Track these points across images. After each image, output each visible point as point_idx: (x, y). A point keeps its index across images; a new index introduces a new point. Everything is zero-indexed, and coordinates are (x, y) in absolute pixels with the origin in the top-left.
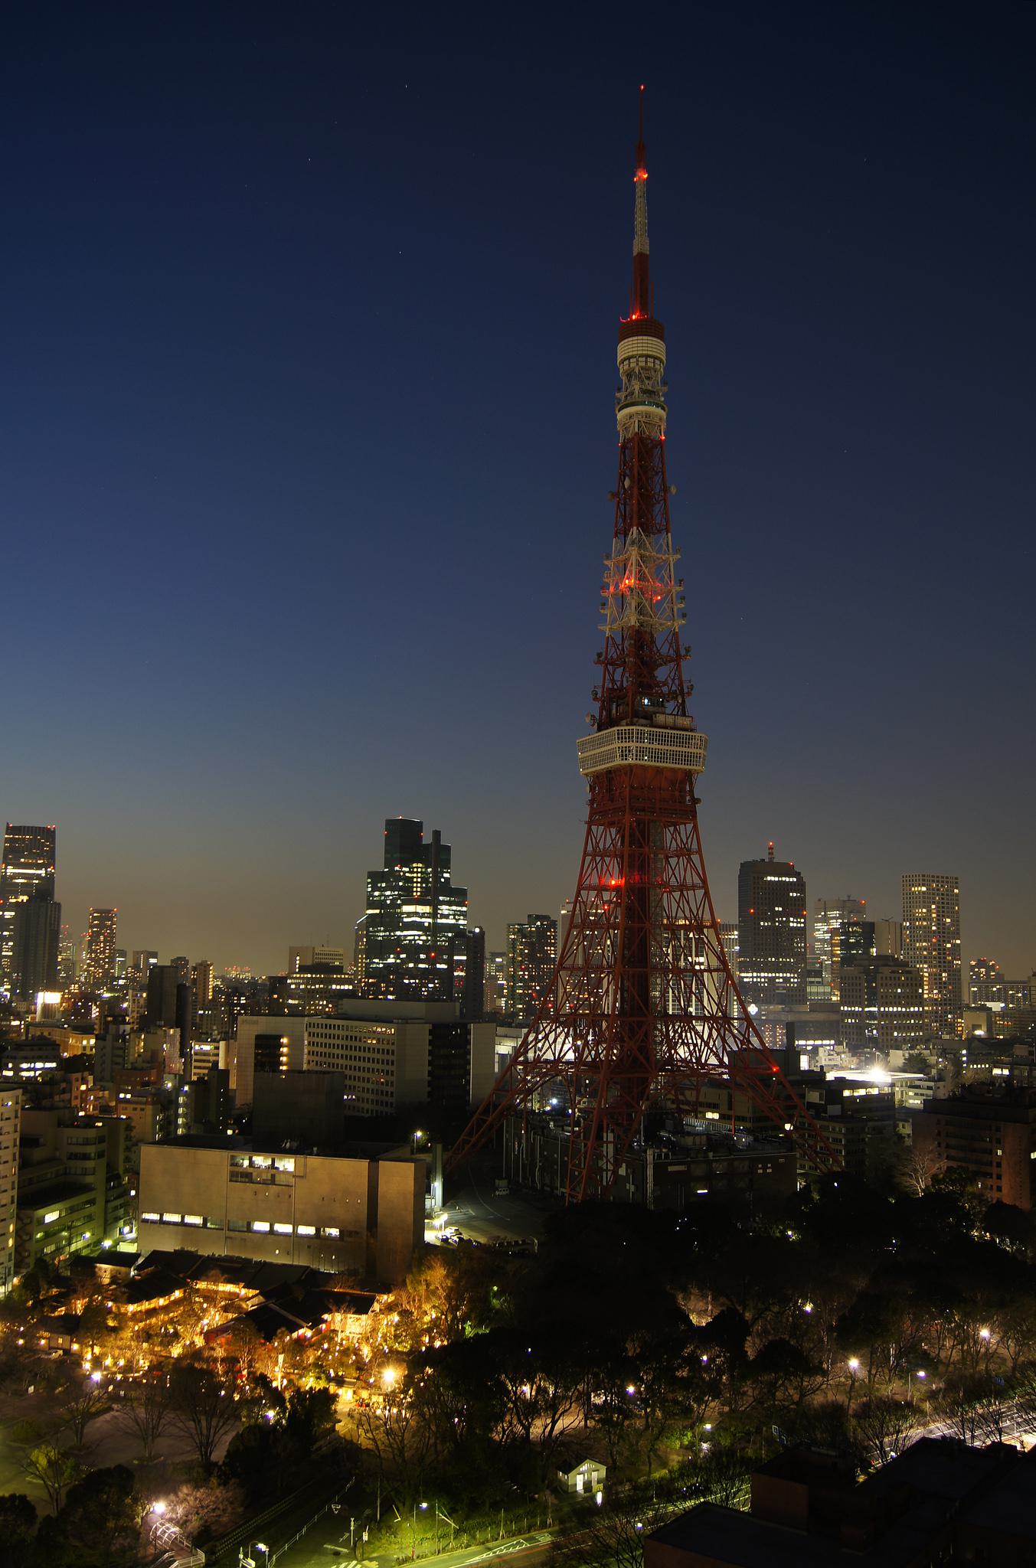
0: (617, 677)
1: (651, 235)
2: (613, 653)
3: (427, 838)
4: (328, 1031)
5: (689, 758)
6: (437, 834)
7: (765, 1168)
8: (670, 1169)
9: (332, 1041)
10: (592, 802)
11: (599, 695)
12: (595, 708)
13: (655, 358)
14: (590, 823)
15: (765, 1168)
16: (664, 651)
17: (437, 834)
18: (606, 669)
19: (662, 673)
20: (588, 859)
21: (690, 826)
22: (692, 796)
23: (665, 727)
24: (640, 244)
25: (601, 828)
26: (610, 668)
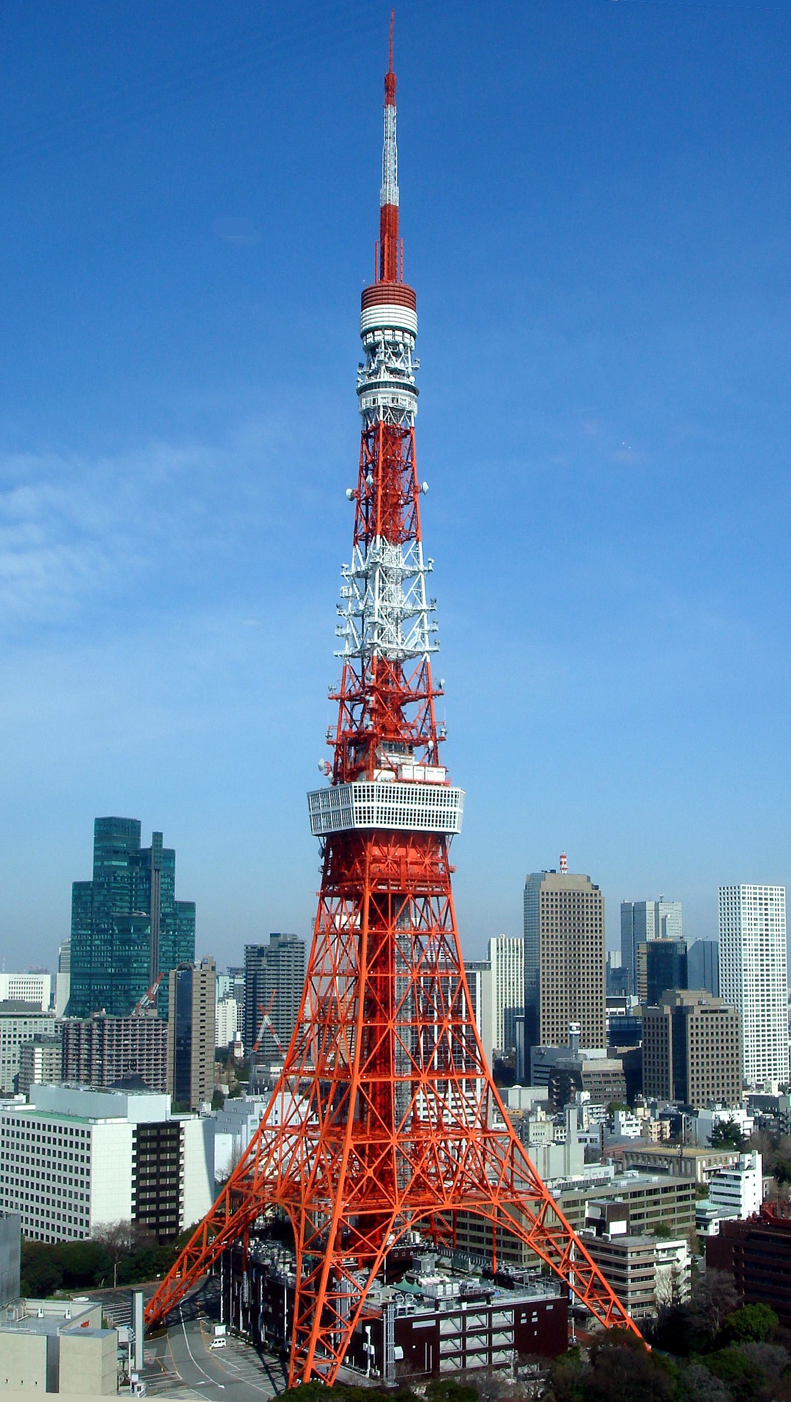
0: (357, 716)
1: (401, 182)
2: (354, 687)
3: (146, 843)
4: (63, 1161)
5: (441, 818)
6: (158, 837)
7: (529, 1317)
8: (416, 1325)
9: (68, 1213)
10: (325, 868)
11: (334, 739)
12: (328, 755)
13: (404, 330)
14: (322, 897)
15: (529, 1317)
16: (413, 686)
17: (158, 837)
18: (342, 705)
19: (412, 712)
20: (321, 938)
21: (443, 900)
22: (446, 865)
23: (411, 782)
24: (392, 194)
25: (337, 900)
26: (348, 703)
